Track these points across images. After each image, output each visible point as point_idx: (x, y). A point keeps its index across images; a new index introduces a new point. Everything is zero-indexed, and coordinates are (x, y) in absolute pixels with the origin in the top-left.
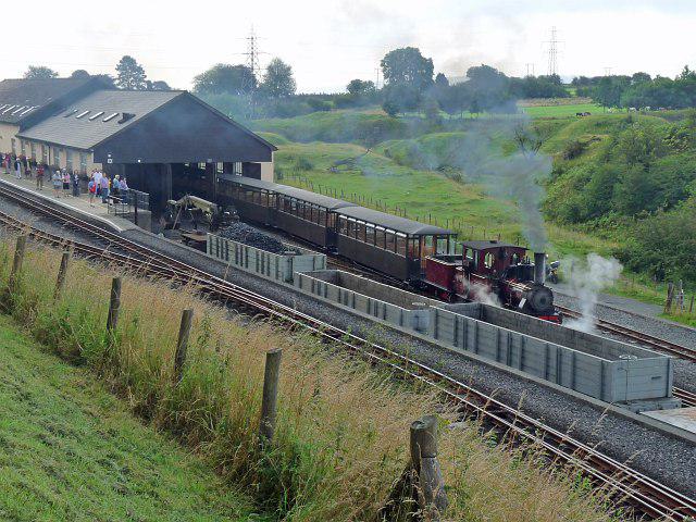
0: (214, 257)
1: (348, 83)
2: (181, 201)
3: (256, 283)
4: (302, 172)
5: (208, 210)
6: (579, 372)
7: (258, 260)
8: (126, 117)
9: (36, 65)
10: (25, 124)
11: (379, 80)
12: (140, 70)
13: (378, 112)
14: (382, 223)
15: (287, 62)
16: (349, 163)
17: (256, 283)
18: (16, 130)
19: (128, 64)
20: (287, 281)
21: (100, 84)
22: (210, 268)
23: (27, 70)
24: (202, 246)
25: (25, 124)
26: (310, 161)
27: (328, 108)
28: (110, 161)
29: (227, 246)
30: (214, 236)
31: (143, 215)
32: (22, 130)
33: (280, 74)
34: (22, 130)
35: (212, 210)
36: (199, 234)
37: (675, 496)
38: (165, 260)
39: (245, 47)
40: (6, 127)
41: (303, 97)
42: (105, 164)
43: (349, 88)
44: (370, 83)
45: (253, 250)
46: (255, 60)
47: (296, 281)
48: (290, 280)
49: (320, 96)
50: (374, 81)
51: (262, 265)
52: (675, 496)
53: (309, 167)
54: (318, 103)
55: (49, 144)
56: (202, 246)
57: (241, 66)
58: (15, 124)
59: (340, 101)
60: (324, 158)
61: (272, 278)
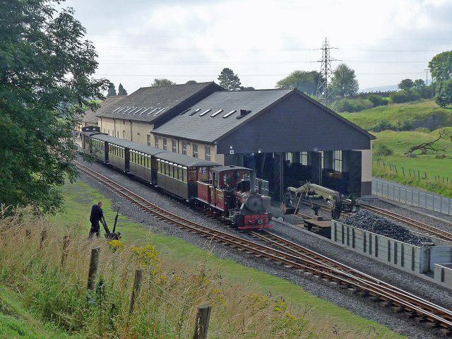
0: (339, 243)
1: (399, 82)
2: (301, 188)
3: (399, 277)
4: (383, 157)
5: (330, 197)
6: (379, 247)
7: (389, 249)
8: (244, 113)
9: (160, 78)
10: (159, 122)
11: (428, 79)
12: (236, 78)
13: (431, 106)
14: (168, 159)
15: (351, 67)
16: (424, 147)
17: (399, 277)
18: (150, 128)
19: (227, 73)
20: (425, 273)
21: (210, 89)
22: (343, 257)
23: (153, 82)
24: (326, 232)
25: (159, 122)
26: (389, 147)
27: (386, 103)
28: (232, 152)
29: (354, 233)
30: (339, 225)
31: (266, 200)
32: (155, 128)
33: (346, 76)
34: (155, 128)
35: (334, 198)
36: (320, 219)
37: (404, 293)
38: (296, 248)
39: (320, 55)
40: (142, 124)
41: (364, 96)
42: (227, 154)
43: (401, 86)
44: (421, 82)
45: (383, 240)
46: (328, 66)
47: (438, 274)
48: (428, 271)
49: (376, 93)
50: (424, 79)
51: (393, 253)
52: (404, 293)
53: (389, 153)
54: (377, 99)
55: (178, 139)
56: (326, 232)
57: (314, 72)
58: (150, 123)
59: (398, 99)
60: (400, 144)
61: (408, 267)
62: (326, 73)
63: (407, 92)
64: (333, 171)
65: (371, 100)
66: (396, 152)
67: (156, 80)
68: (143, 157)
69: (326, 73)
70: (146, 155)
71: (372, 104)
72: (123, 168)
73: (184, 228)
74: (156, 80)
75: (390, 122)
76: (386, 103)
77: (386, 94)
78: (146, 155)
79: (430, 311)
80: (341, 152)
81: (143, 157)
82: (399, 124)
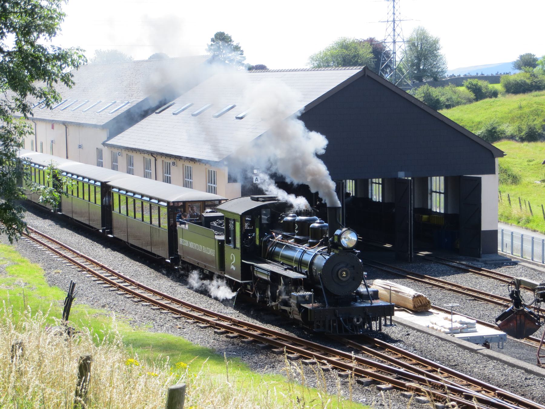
1: (515, 57)
15: (433, 33)
27: (495, 94)
46: (398, 30)
62: (394, 42)
63: (528, 75)
64: (430, 212)
65: (468, 88)
66: (539, 182)
67: (97, 51)
68: (37, 170)
69: (394, 42)
70: (37, 166)
71: (472, 96)
72: (97, 224)
73: (199, 320)
74: (97, 51)
75: (503, 127)
76: (495, 94)
77: (495, 79)
78: (37, 166)
79: (423, 375)
80: (442, 178)
81: (37, 170)
82: (520, 130)
